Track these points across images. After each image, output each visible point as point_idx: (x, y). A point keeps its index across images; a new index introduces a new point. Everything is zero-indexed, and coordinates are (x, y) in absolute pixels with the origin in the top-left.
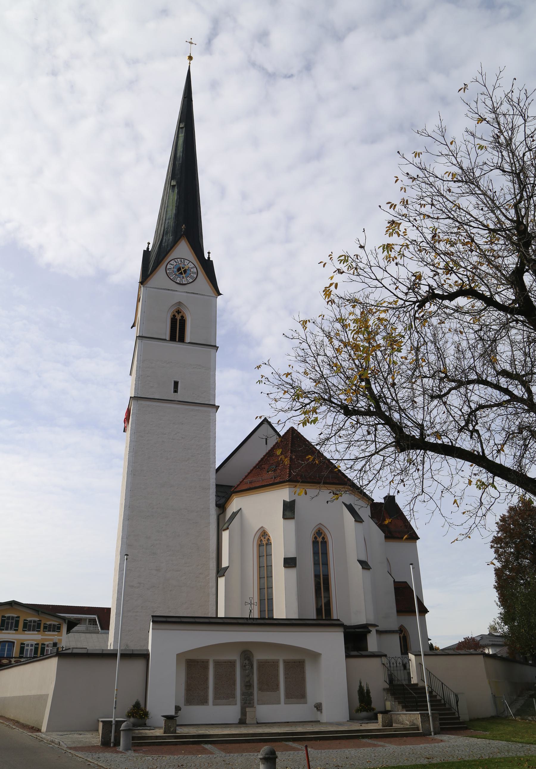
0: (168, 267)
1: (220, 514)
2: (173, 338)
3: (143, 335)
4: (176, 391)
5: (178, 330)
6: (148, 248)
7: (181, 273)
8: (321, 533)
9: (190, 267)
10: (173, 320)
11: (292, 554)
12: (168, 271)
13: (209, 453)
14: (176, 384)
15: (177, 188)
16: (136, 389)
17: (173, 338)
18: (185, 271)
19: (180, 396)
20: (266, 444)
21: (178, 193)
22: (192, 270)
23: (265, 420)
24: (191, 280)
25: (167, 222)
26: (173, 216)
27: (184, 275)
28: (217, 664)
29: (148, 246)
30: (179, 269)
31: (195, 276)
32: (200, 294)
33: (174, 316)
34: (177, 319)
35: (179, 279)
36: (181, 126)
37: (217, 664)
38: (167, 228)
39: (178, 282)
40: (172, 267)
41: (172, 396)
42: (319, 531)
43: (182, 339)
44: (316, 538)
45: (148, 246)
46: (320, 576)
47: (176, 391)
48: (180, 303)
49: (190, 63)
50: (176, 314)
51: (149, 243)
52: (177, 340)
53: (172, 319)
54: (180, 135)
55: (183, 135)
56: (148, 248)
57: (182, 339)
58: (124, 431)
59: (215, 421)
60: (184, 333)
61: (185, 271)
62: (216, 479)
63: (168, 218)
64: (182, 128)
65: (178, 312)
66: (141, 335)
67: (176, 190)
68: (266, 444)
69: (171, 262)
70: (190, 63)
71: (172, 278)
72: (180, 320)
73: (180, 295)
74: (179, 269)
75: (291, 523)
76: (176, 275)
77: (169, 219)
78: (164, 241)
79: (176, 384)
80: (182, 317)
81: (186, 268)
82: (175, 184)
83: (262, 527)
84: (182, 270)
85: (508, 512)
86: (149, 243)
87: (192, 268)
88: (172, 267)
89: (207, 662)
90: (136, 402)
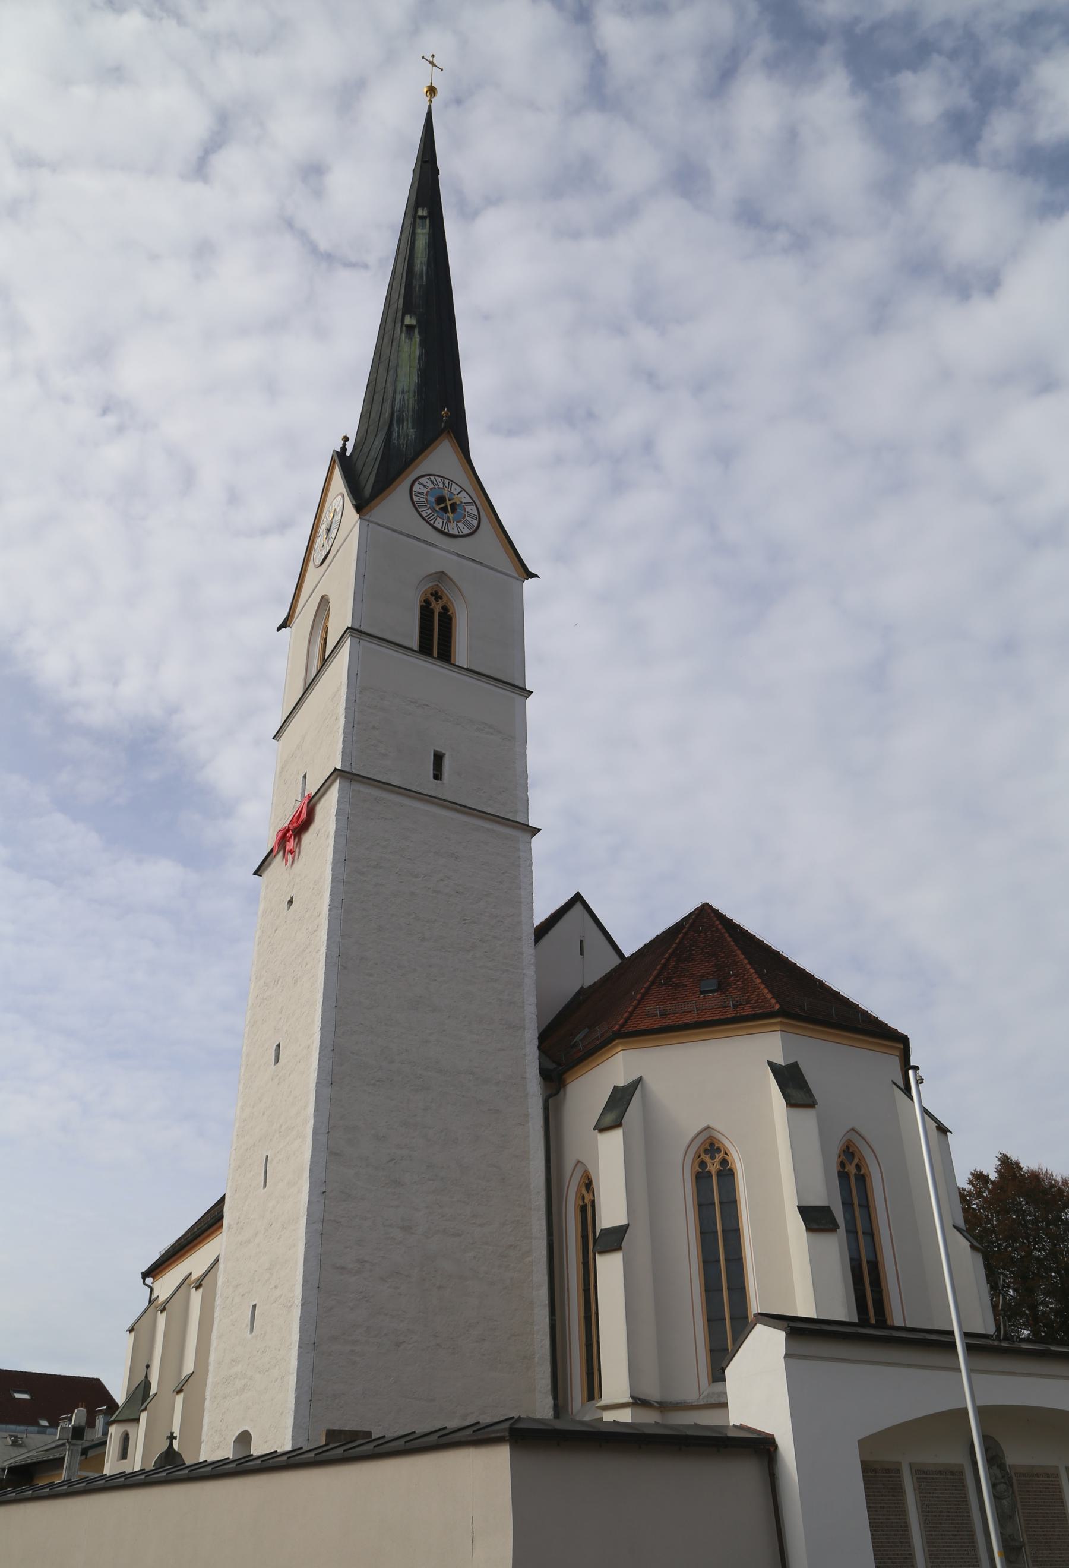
0: (416, 488)
1: (550, 1096)
2: (425, 649)
3: (363, 629)
4: (437, 777)
5: (435, 635)
6: (344, 449)
7: (445, 510)
8: (853, 1154)
9: (464, 501)
10: (426, 612)
11: (818, 1199)
12: (415, 498)
13: (520, 939)
14: (438, 758)
15: (419, 333)
16: (347, 753)
17: (425, 649)
18: (454, 507)
19: (450, 786)
20: (582, 953)
21: (422, 343)
22: (468, 508)
23: (578, 898)
24: (466, 531)
25: (398, 397)
26: (412, 388)
27: (450, 514)
28: (922, 1474)
29: (344, 445)
30: (441, 500)
31: (475, 523)
32: (487, 566)
33: (427, 601)
34: (432, 612)
35: (439, 520)
36: (420, 213)
37: (922, 1474)
38: (401, 411)
39: (439, 527)
40: (425, 490)
41: (426, 783)
42: (848, 1147)
43: (445, 655)
44: (842, 1164)
45: (344, 445)
46: (860, 1260)
47: (437, 777)
48: (442, 575)
49: (430, 101)
50: (432, 600)
51: (346, 439)
52: (435, 654)
53: (422, 608)
54: (419, 231)
55: (426, 231)
56: (344, 449)
57: (445, 655)
58: (256, 873)
59: (531, 865)
60: (450, 647)
61: (454, 507)
62: (537, 1005)
63: (400, 388)
64: (422, 218)
65: (437, 596)
66: (357, 627)
67: (417, 338)
68: (582, 953)
69: (424, 480)
70: (430, 101)
71: (424, 514)
72: (440, 613)
73: (442, 556)
74: (441, 500)
75: (807, 1117)
76: (434, 510)
77: (403, 392)
78: (395, 434)
79: (438, 758)
80: (445, 609)
81: (456, 500)
82: (414, 322)
83: (708, 1127)
84: (448, 503)
85: (970, 1182)
86: (346, 439)
87: (468, 504)
88: (425, 490)
89: (899, 1463)
90: (347, 784)
